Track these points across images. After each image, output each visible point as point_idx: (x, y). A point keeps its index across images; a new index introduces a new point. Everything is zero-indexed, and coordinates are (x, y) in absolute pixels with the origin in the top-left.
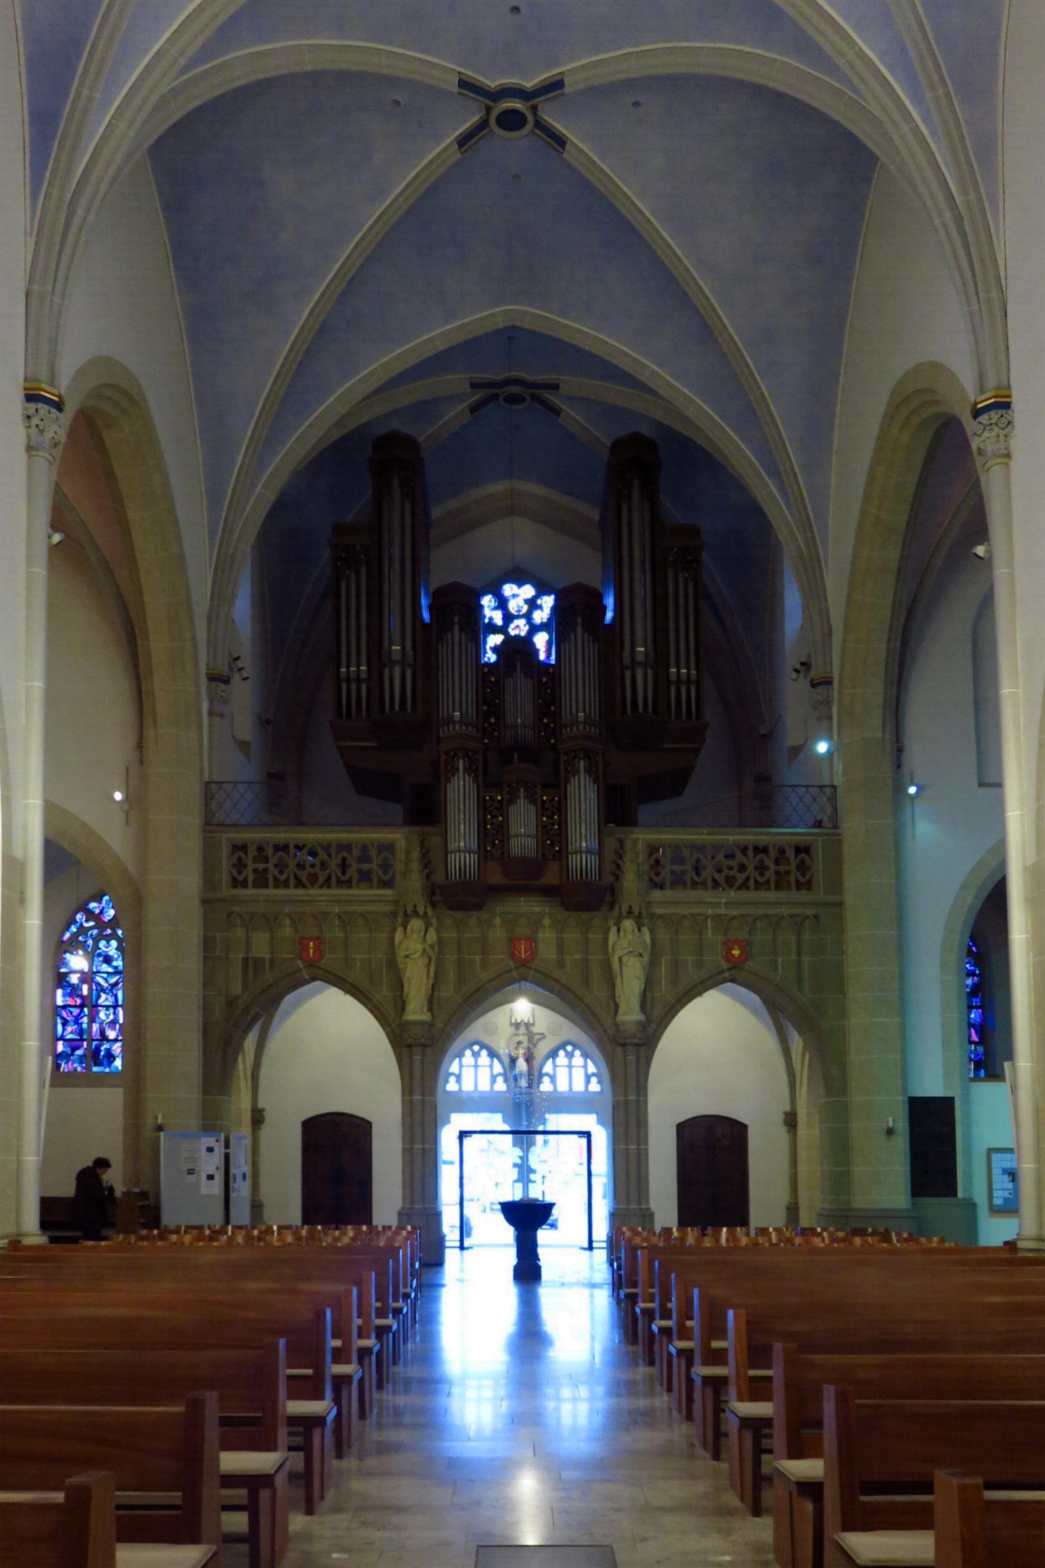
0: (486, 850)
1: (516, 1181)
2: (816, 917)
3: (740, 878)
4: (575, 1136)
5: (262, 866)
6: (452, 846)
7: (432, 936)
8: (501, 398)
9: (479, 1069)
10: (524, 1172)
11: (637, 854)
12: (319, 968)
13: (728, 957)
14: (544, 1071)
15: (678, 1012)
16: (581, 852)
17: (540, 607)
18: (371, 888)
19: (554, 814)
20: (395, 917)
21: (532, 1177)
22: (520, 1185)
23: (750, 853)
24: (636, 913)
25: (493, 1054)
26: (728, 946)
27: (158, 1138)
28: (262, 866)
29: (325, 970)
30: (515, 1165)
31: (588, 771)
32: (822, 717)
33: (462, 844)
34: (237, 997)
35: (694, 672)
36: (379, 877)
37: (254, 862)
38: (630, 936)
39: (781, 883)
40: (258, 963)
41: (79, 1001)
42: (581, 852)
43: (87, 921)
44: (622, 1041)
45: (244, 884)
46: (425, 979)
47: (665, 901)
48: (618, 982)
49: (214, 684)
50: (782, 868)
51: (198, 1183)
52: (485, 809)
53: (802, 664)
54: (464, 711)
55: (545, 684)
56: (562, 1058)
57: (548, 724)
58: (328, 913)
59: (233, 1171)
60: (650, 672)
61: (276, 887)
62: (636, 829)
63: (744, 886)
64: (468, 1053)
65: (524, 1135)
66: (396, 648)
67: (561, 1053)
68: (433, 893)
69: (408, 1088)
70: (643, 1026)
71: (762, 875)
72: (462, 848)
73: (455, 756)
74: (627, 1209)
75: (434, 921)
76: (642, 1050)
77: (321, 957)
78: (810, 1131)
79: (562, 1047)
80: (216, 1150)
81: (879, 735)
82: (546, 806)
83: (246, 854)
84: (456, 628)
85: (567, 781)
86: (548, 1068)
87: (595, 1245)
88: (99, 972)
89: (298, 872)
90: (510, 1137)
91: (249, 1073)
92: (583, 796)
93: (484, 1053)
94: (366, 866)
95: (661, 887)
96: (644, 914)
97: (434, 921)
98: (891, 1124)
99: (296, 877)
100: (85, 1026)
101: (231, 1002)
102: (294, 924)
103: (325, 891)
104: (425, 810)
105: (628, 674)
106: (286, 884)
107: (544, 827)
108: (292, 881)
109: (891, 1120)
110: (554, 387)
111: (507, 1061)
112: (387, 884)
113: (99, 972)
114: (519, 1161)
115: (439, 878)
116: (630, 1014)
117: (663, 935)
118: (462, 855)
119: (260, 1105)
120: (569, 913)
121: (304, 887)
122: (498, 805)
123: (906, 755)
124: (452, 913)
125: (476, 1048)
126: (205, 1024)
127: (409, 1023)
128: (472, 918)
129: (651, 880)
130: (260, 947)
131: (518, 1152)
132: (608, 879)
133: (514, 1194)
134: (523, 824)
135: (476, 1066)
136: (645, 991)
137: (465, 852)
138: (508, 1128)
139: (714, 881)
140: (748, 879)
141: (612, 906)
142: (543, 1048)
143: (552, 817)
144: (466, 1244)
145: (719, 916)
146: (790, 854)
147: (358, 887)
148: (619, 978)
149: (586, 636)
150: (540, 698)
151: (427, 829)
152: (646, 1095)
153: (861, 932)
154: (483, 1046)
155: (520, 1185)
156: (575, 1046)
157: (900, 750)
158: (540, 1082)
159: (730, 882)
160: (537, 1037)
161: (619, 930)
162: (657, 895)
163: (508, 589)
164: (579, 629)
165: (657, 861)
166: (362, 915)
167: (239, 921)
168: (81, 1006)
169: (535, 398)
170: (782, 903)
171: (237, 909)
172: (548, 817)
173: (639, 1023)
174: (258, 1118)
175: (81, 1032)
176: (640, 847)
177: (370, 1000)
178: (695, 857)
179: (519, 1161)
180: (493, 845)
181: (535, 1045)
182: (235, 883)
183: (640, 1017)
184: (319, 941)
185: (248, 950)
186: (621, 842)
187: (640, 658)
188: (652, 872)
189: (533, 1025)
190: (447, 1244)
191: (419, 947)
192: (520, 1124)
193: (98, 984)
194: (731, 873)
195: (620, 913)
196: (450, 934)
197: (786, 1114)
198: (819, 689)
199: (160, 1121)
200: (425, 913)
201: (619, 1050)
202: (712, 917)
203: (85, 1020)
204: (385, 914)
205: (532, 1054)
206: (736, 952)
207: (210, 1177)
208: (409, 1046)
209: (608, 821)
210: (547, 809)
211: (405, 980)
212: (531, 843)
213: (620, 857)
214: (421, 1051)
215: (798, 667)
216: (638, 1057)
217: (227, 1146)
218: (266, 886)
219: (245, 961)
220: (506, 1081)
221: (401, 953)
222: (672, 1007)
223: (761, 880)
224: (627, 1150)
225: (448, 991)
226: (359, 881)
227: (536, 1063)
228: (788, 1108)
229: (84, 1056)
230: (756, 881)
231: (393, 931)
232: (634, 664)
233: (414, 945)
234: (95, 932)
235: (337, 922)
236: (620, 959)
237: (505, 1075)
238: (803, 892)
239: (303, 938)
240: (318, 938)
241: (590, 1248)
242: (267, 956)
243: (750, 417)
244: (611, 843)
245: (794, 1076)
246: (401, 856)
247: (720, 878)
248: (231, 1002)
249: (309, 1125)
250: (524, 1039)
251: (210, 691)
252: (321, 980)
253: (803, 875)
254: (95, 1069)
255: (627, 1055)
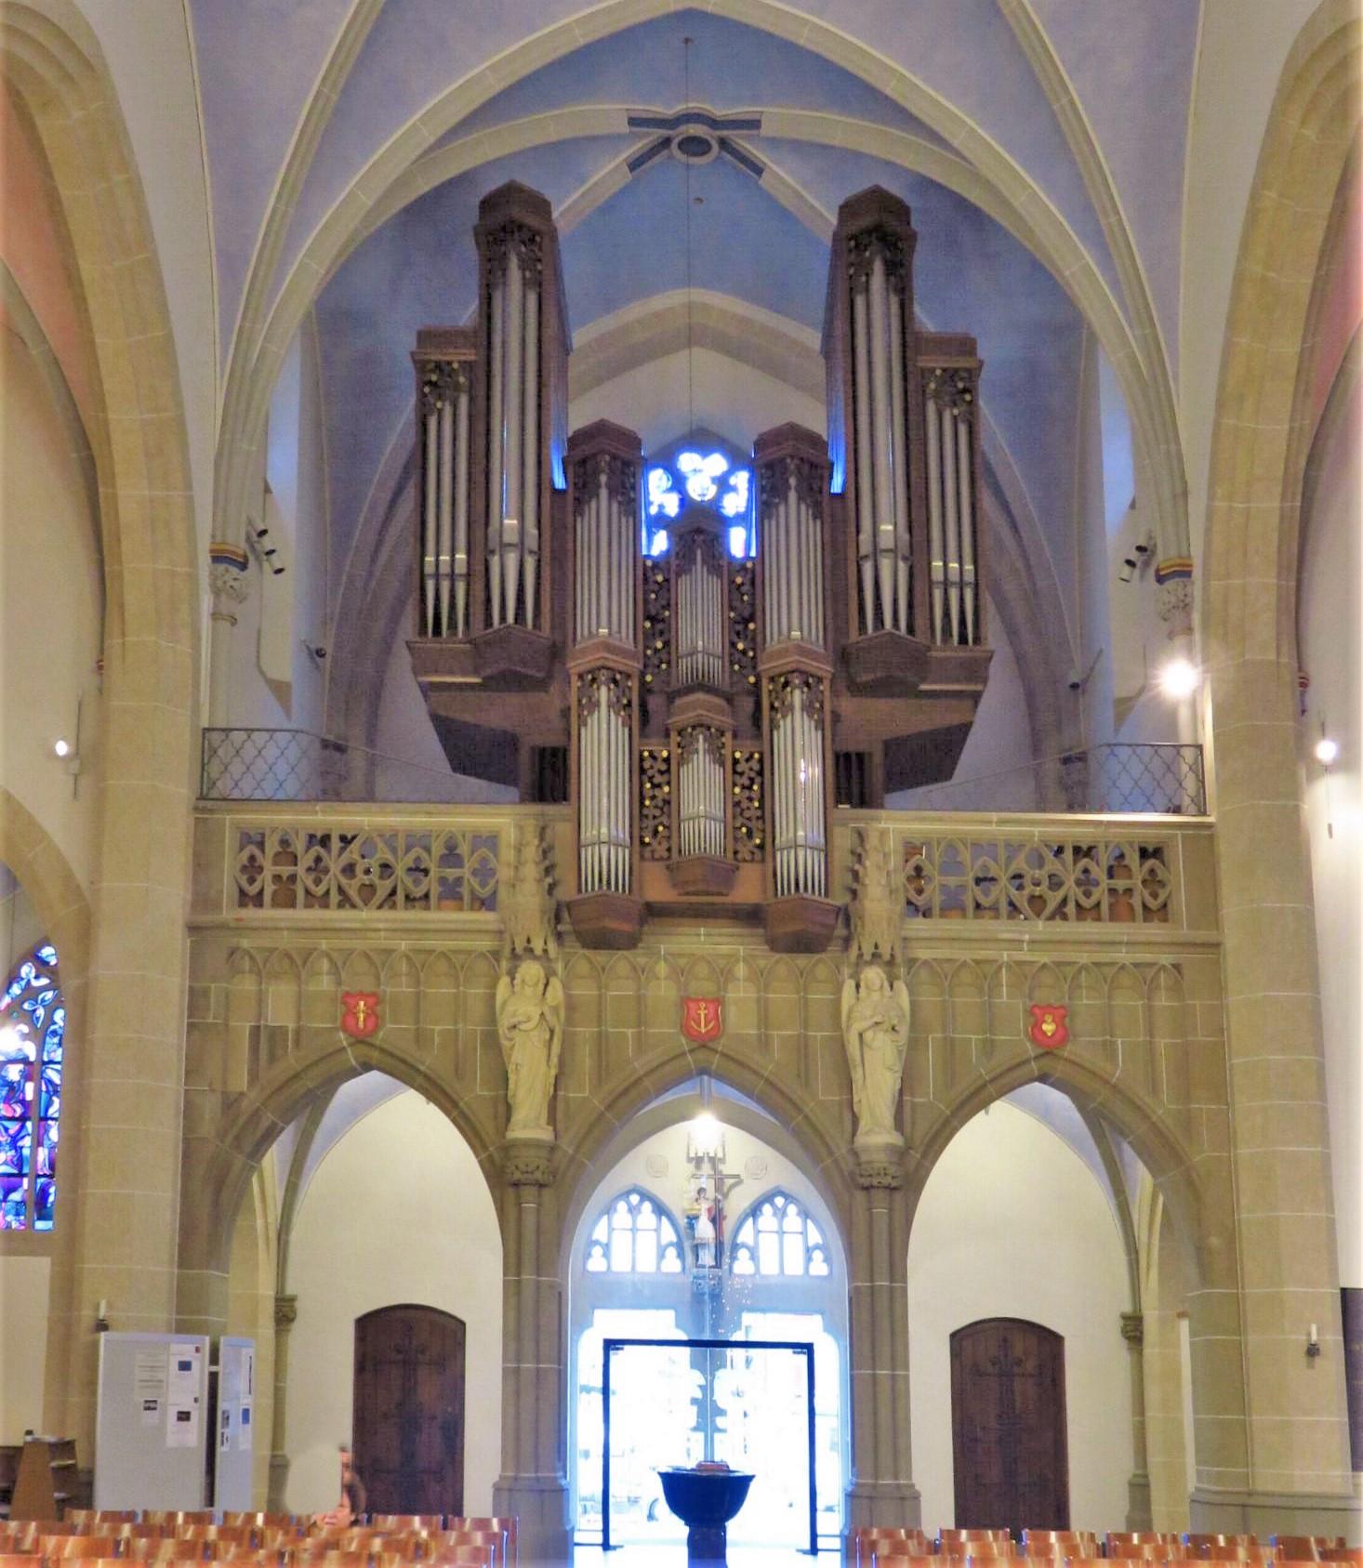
0: (642, 843)
1: (695, 1429)
2: (1177, 967)
3: (1053, 899)
4: (790, 1351)
5: (286, 871)
6: (588, 834)
7: (556, 992)
8: (675, 142)
9: (639, 1234)
10: (708, 1413)
11: (886, 855)
12: (372, 1045)
13: (1036, 1034)
14: (740, 1240)
15: (955, 1130)
16: (796, 846)
17: (734, 489)
18: (461, 909)
19: (752, 780)
20: (498, 961)
21: (720, 1421)
22: (700, 1436)
23: (1068, 855)
24: (887, 957)
25: (660, 1210)
26: (1036, 1014)
27: (95, 1345)
28: (286, 871)
29: (382, 1050)
30: (694, 1401)
31: (808, 708)
32: (1175, 624)
33: (604, 830)
34: (242, 1094)
35: (969, 567)
36: (472, 892)
37: (275, 863)
38: (876, 996)
39: (1119, 907)
40: (276, 1034)
41: (19, 1110)
42: (796, 846)
43: (37, 977)
44: (864, 1181)
45: (258, 900)
46: (543, 1067)
47: (937, 938)
48: (857, 1075)
49: (221, 567)
50: (1120, 884)
51: (161, 1429)
52: (642, 771)
53: (1140, 549)
54: (615, 628)
55: (740, 586)
56: (767, 1217)
57: (744, 652)
58: (389, 952)
59: (222, 1405)
60: (902, 567)
61: (308, 906)
62: (883, 813)
63: (1060, 913)
64: (622, 1206)
65: (709, 1347)
66: (510, 522)
67: (767, 1208)
68: (558, 919)
69: (514, 1263)
70: (901, 1154)
71: (1088, 894)
72: (604, 838)
73: (594, 680)
74: (874, 1486)
75: (559, 967)
76: (898, 1196)
77: (377, 1027)
78: (1176, 1345)
79: (768, 1198)
80: (195, 1366)
81: (1272, 656)
82: (739, 769)
83: (263, 851)
84: (604, 493)
85: (774, 726)
86: (746, 1235)
87: (821, 1543)
88: (51, 1062)
89: (344, 881)
90: (687, 1351)
91: (273, 1235)
92: (803, 768)
93: (647, 1206)
94: (452, 873)
95: (926, 914)
96: (899, 959)
97: (559, 967)
98: (1314, 1338)
99: (341, 890)
100: (26, 1152)
101: (230, 1103)
102: (335, 970)
103: (386, 914)
104: (550, 778)
105: (868, 568)
106: (324, 902)
107: (737, 804)
108: (335, 897)
109: (1314, 1329)
110: (754, 124)
111: (683, 1222)
112: (487, 903)
113: (51, 1062)
114: (699, 1395)
115: (566, 892)
116: (878, 1134)
117: (929, 998)
118: (604, 849)
119: (290, 1290)
120: (778, 956)
121: (354, 906)
122: (664, 767)
123: (1311, 689)
124: (586, 952)
125: (635, 1199)
126: (186, 1141)
127: (515, 1144)
128: (619, 961)
129: (909, 903)
130: (280, 1014)
131: (698, 1378)
132: (840, 899)
133: (688, 1457)
134: (702, 792)
135: (634, 1230)
136: (901, 1092)
137: (608, 843)
138: (684, 1337)
139: (1011, 904)
140: (1064, 902)
141: (847, 941)
142: (737, 1203)
143: (750, 788)
144: (612, 1542)
145: (1019, 963)
146: (1133, 859)
147: (439, 908)
148: (860, 1070)
149: (803, 507)
150: (732, 608)
151: (551, 809)
152: (904, 1279)
153: (1248, 992)
154: (645, 1196)
155: (700, 1436)
156: (789, 1198)
157: (1304, 684)
158: (733, 1258)
159: (1037, 902)
160: (729, 1182)
161: (858, 986)
162: (918, 926)
163: (687, 461)
164: (792, 496)
165: (918, 869)
166: (443, 954)
167: (247, 964)
168: (23, 1119)
169: (723, 143)
170: (1121, 943)
171: (245, 943)
172: (743, 787)
173: (890, 1148)
174: (285, 1313)
175: (19, 1162)
176: (892, 844)
177: (455, 1104)
178: (980, 862)
179: (699, 1395)
180: (656, 832)
181: (726, 1196)
182: (244, 899)
183: (895, 1139)
184: (374, 999)
185: (259, 1016)
186: (861, 836)
187: (886, 542)
188: (911, 888)
189: (722, 1161)
190: (578, 1537)
191: (535, 1012)
192: (702, 1330)
193: (50, 1082)
194: (1037, 891)
195: (860, 956)
196: (585, 991)
197: (1125, 1317)
198: (1170, 584)
199: (102, 1313)
200: (545, 951)
201: (860, 1196)
202: (1009, 967)
203: (27, 1142)
204: (482, 955)
205: (720, 1211)
206: (1049, 1028)
207: (184, 1416)
208: (516, 1185)
209: (838, 802)
210: (741, 774)
211: (511, 1068)
212: (715, 829)
213: (859, 858)
214: (537, 1194)
215: (1134, 556)
216: (891, 1210)
217: (214, 1359)
218: (293, 905)
219: (256, 1031)
220: (681, 1255)
221: (504, 1023)
222: (946, 1123)
223: (1086, 903)
224: (874, 1376)
225: (580, 1091)
226: (441, 898)
227: (728, 1226)
228: (1127, 1308)
229: (23, 1202)
230: (1078, 905)
231: (493, 985)
232: (876, 552)
233: (526, 1003)
234: (49, 995)
235: (404, 968)
236: (861, 1035)
237: (679, 1246)
238: (1156, 923)
239: (347, 994)
240: (374, 995)
241: (814, 1550)
242: (291, 1025)
243: (1055, 146)
244: (843, 840)
245: (1137, 1252)
246: (507, 854)
247: (1021, 899)
248: (230, 1103)
249: (370, 1326)
250: (709, 1185)
251: (214, 577)
252: (380, 1069)
253: (1155, 896)
254: (40, 1225)
255: (874, 1203)
